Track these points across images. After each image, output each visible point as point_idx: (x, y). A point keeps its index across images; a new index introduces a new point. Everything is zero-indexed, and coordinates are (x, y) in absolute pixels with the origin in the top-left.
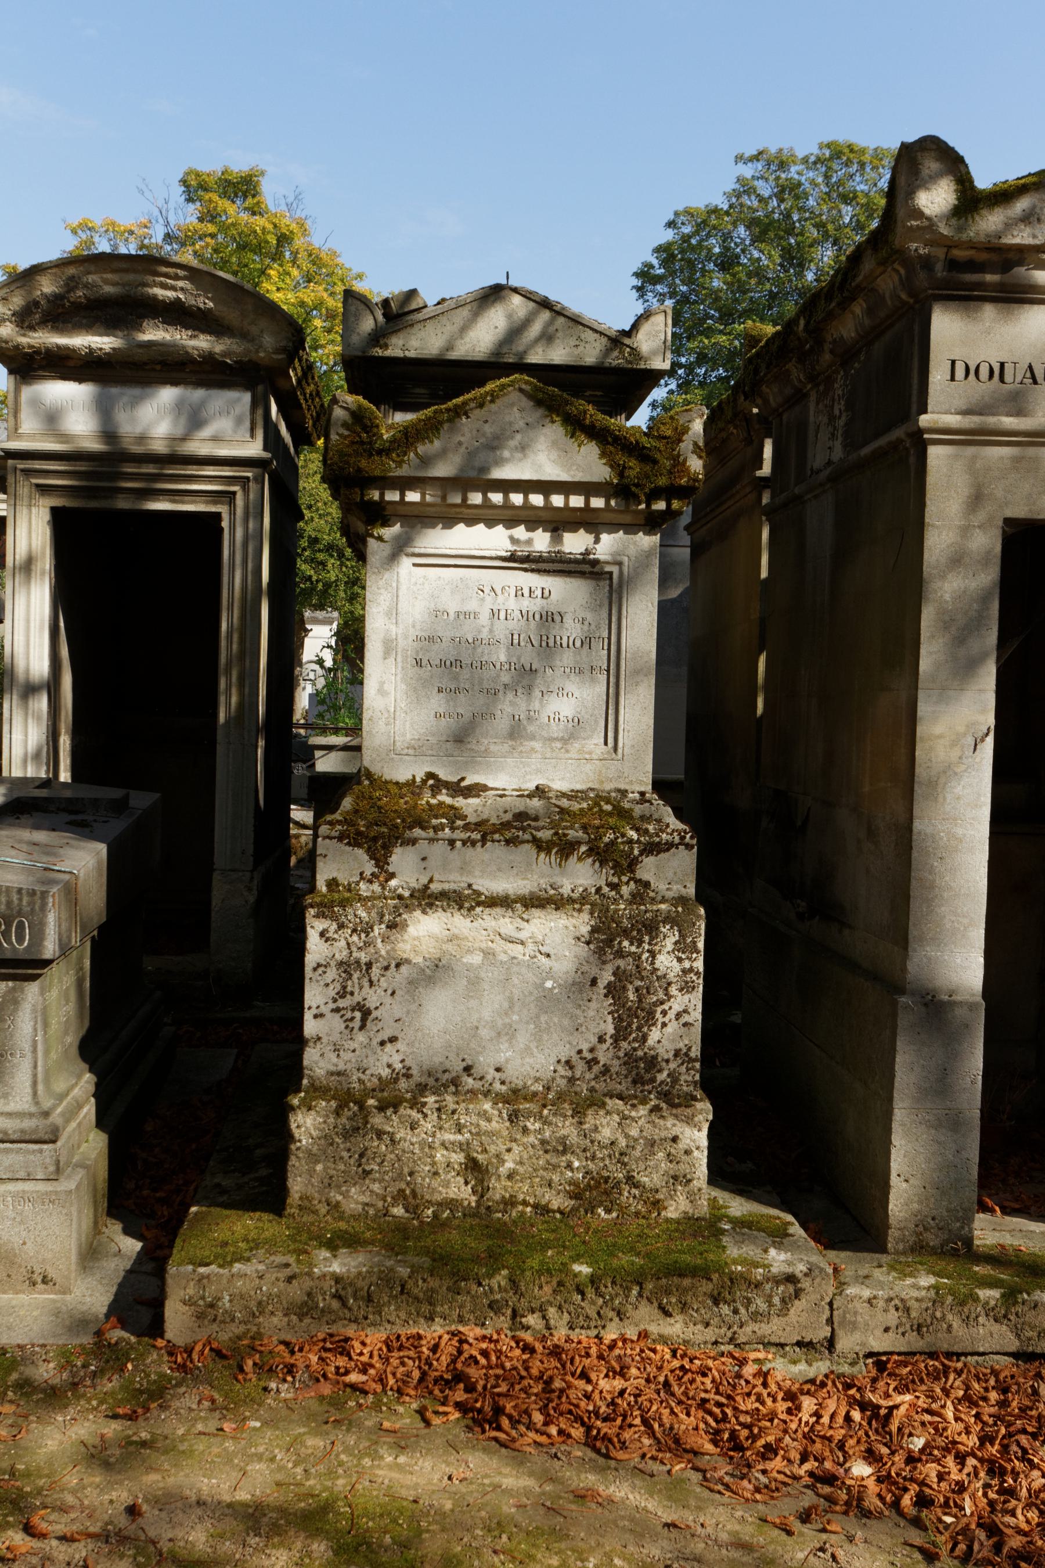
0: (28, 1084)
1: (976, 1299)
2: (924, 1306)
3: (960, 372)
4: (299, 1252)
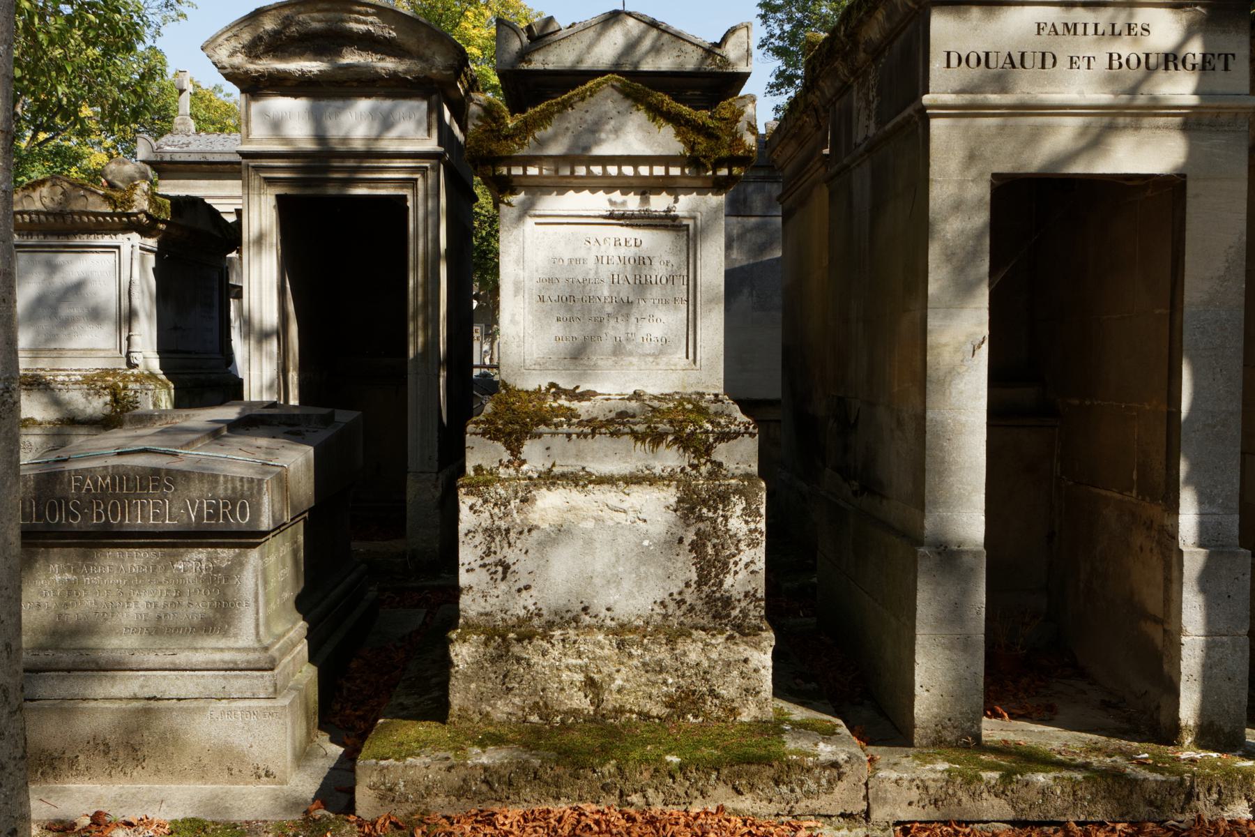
0: (252, 626)
1: (980, 779)
2: (939, 785)
3: (954, 61)
4: (457, 749)
